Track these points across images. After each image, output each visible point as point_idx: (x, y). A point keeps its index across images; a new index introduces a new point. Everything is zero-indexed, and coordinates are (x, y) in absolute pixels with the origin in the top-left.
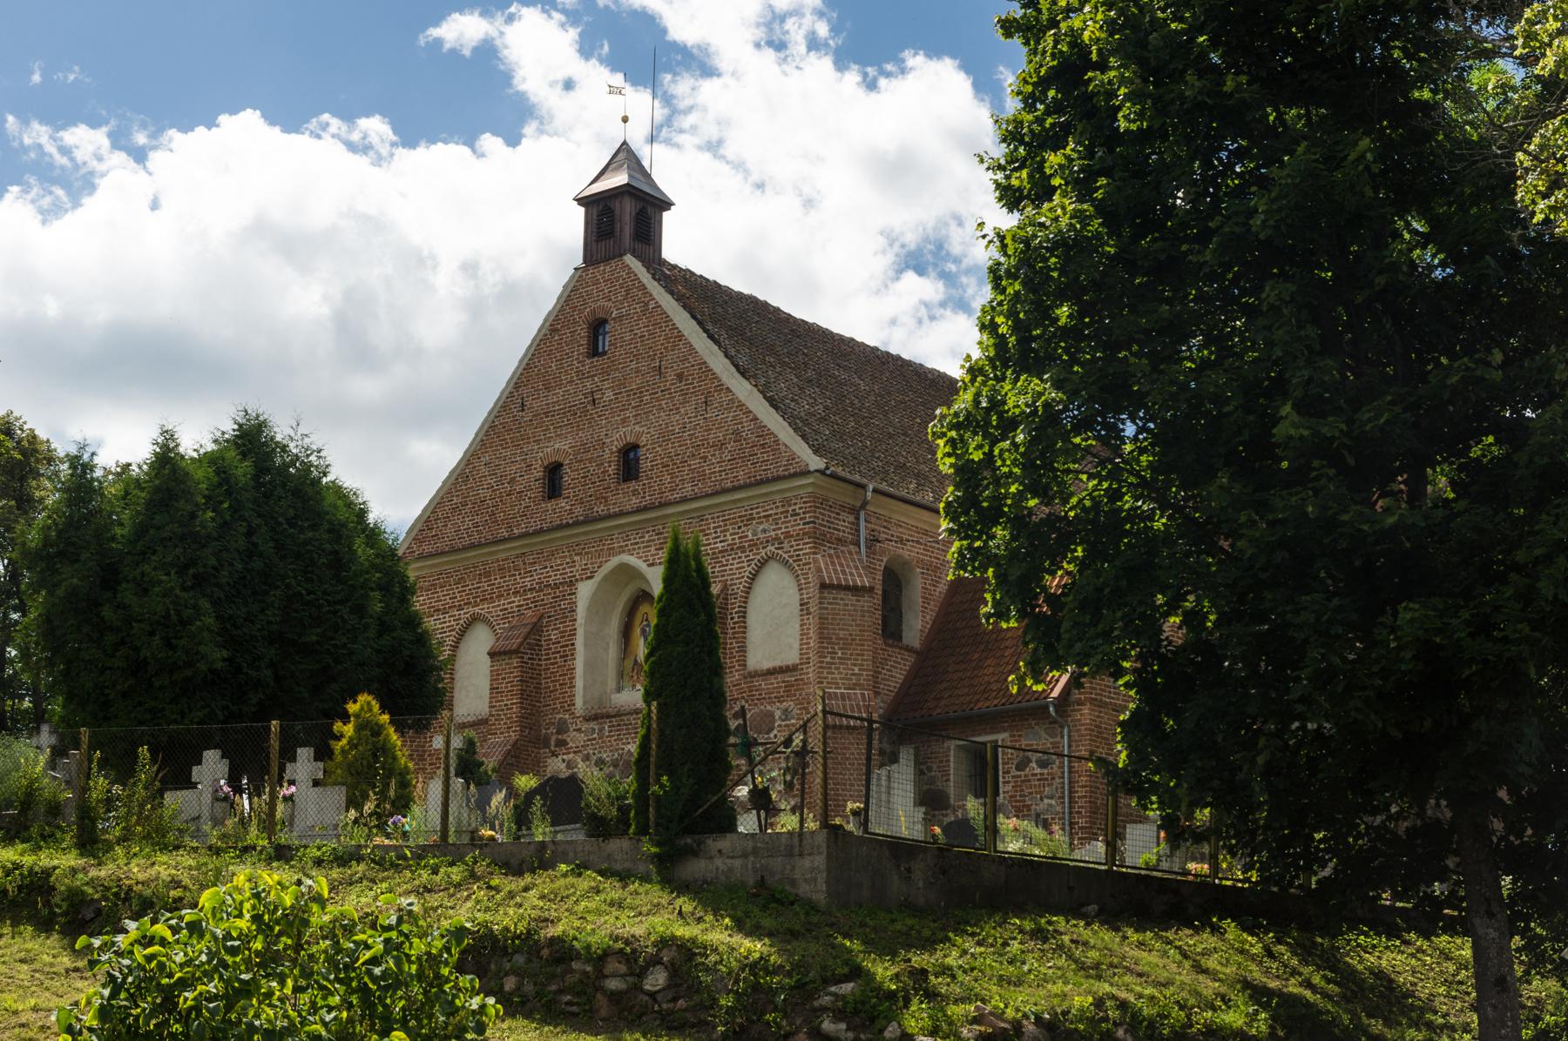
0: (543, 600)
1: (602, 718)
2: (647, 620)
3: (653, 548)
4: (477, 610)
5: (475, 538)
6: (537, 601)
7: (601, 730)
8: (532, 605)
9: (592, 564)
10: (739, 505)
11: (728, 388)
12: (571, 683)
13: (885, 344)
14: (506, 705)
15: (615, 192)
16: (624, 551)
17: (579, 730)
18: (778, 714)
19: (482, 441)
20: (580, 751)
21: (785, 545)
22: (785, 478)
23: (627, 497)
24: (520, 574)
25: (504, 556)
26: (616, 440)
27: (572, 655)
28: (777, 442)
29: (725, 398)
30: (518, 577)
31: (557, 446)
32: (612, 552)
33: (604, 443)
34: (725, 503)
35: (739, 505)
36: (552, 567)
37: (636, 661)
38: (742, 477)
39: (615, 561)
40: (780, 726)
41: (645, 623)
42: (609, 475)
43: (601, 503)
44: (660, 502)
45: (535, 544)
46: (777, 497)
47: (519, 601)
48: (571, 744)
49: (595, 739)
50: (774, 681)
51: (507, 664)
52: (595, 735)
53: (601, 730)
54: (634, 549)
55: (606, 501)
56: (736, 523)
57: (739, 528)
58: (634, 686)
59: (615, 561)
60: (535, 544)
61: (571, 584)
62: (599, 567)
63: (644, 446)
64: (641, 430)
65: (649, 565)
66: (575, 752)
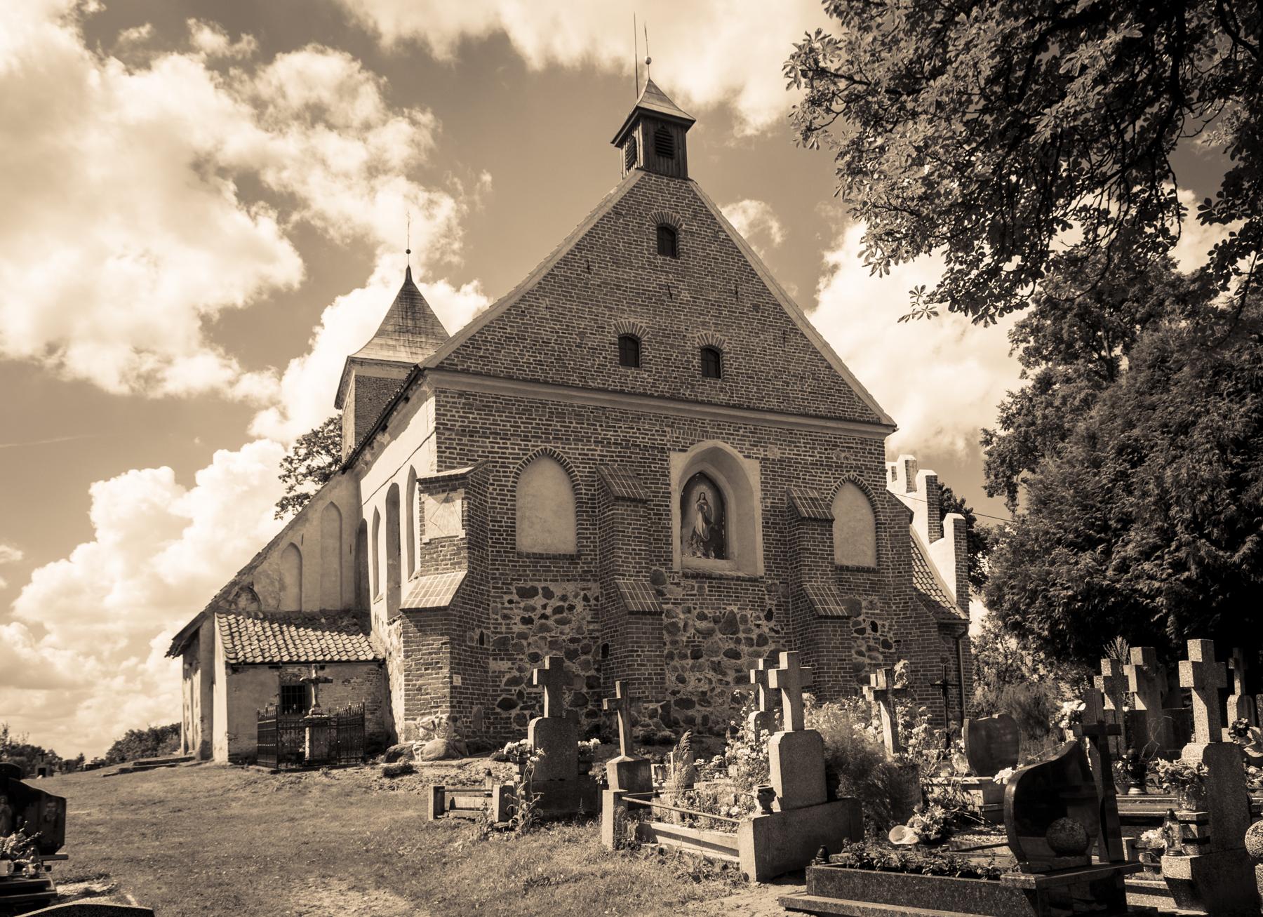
0: (630, 457)
1: (702, 578)
2: (704, 499)
3: (747, 443)
4: (549, 446)
5: (540, 375)
6: (624, 457)
7: (701, 588)
8: (509, 445)
9: (683, 439)
10: (825, 431)
11: (802, 334)
12: (667, 540)
13: (401, 271)
14: (633, 550)
15: (666, 118)
16: (718, 438)
17: (678, 584)
18: (864, 604)
19: (540, 283)
20: (680, 604)
21: (865, 474)
22: (860, 422)
23: (710, 389)
24: (601, 426)
25: (580, 403)
26: (700, 336)
27: (668, 515)
28: (851, 392)
29: (802, 343)
30: (599, 429)
31: (632, 320)
32: (705, 435)
33: (685, 336)
34: (838, 429)
35: (825, 431)
36: (639, 429)
37: (694, 532)
38: (823, 409)
39: (708, 444)
40: (867, 613)
41: (702, 501)
42: (693, 366)
43: (687, 388)
44: (748, 406)
45: (621, 403)
46: (857, 435)
47: (602, 451)
48: (668, 596)
49: (695, 595)
50: (862, 578)
51: (632, 511)
52: (694, 592)
53: (701, 588)
54: (728, 439)
55: (693, 388)
56: (823, 445)
57: (826, 449)
58: (694, 554)
59: (708, 444)
60: (621, 403)
61: (662, 451)
62: (691, 444)
63: (727, 353)
64: (723, 338)
65: (745, 457)
66: (673, 603)
